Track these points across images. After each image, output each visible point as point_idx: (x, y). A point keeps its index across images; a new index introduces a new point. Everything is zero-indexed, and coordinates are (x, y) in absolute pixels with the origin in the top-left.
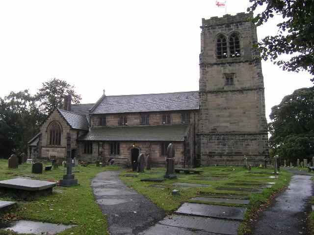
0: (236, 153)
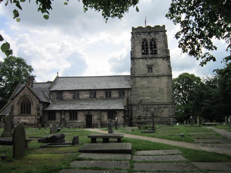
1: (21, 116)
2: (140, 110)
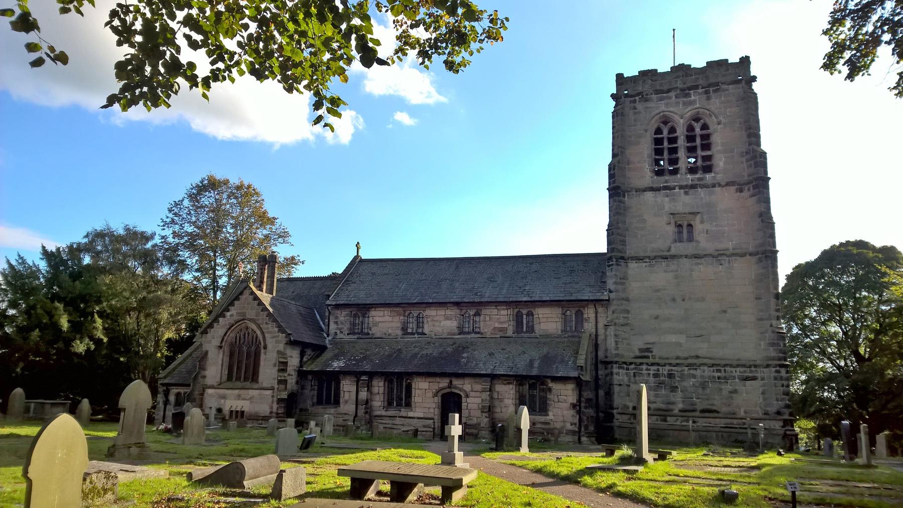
0: (703, 411)
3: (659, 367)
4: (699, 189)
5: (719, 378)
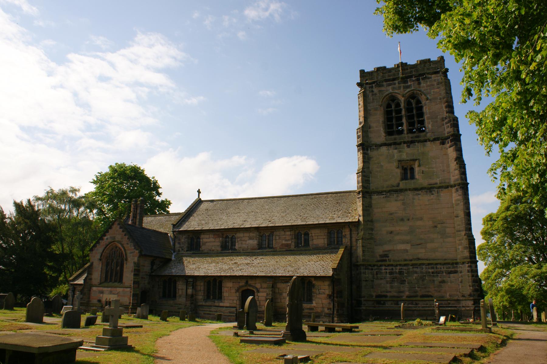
0: (422, 296)
1: (105, 287)
2: (381, 279)
3: (393, 267)
4: (416, 144)
5: (433, 273)
